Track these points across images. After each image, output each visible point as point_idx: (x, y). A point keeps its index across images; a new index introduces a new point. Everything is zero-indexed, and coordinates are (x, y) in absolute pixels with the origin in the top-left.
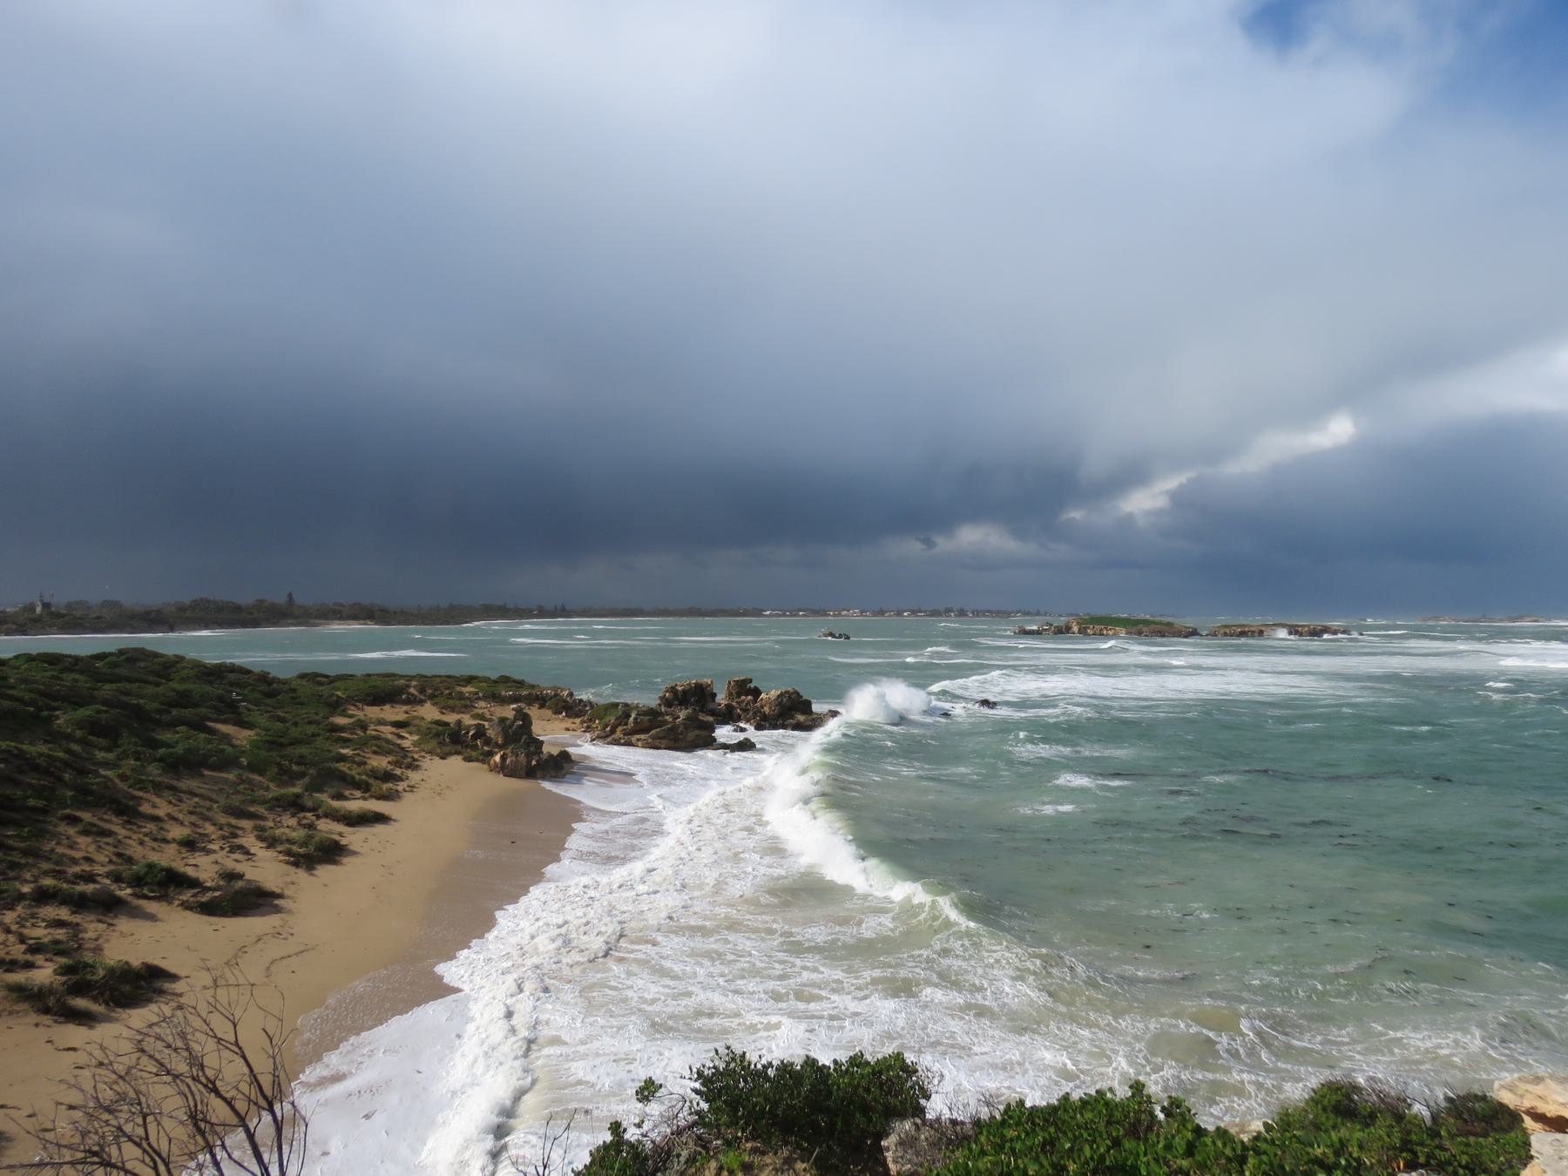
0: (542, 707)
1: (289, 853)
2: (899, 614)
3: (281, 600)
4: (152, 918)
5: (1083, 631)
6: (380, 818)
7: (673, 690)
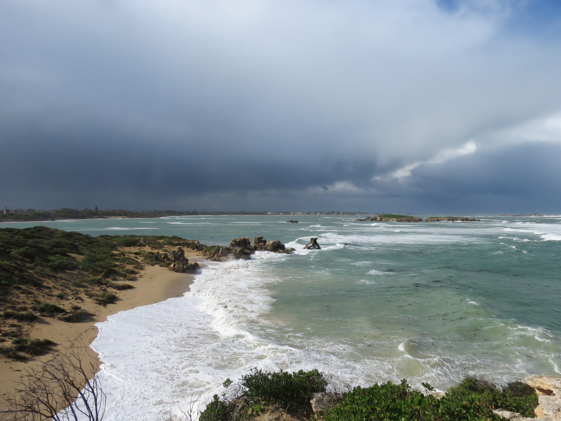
1: (97, 300)
3: (93, 208)
6: (130, 287)
7: (235, 241)
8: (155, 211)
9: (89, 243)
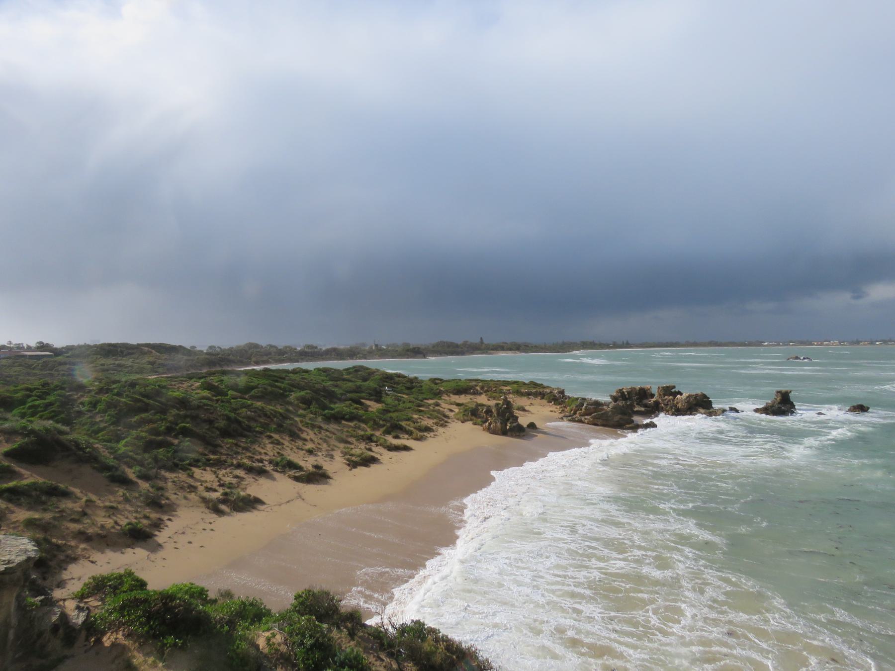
0: (542, 398)
1: (348, 460)
2: (872, 343)
3: (476, 340)
4: (274, 479)
6: (406, 448)
7: (621, 391)
8: (564, 344)
9: (408, 388)
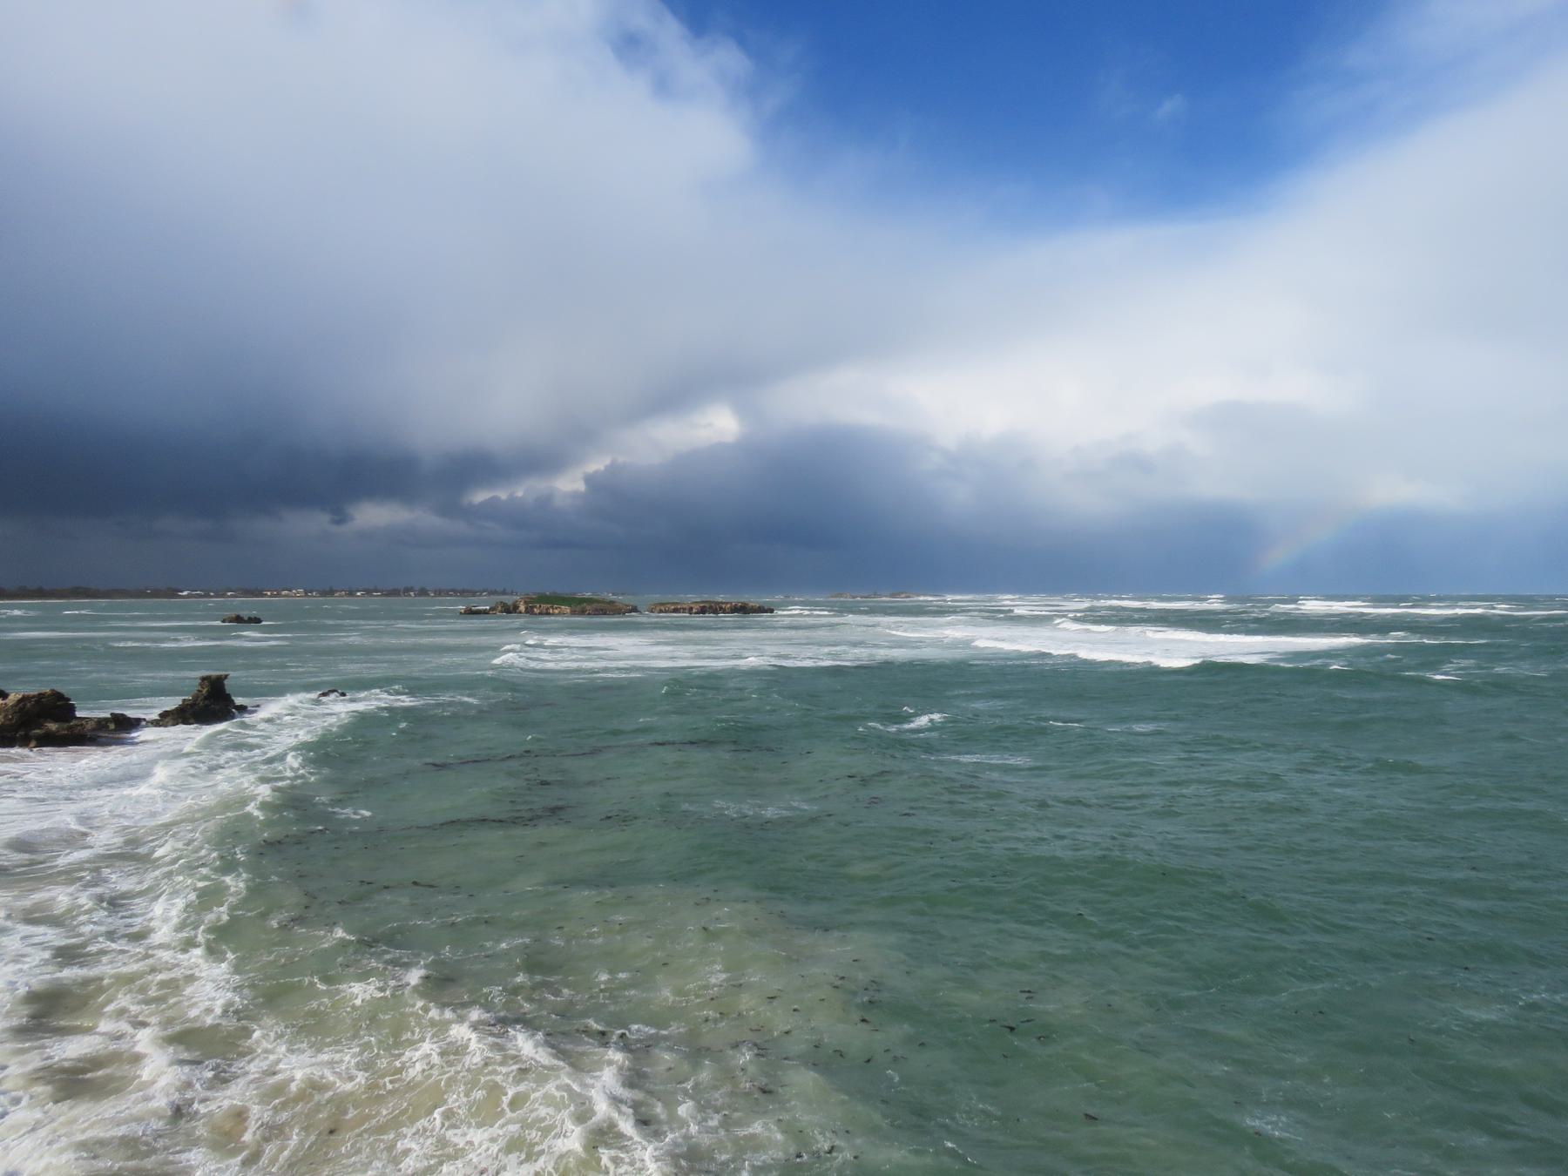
2: (351, 593)
5: (529, 611)
